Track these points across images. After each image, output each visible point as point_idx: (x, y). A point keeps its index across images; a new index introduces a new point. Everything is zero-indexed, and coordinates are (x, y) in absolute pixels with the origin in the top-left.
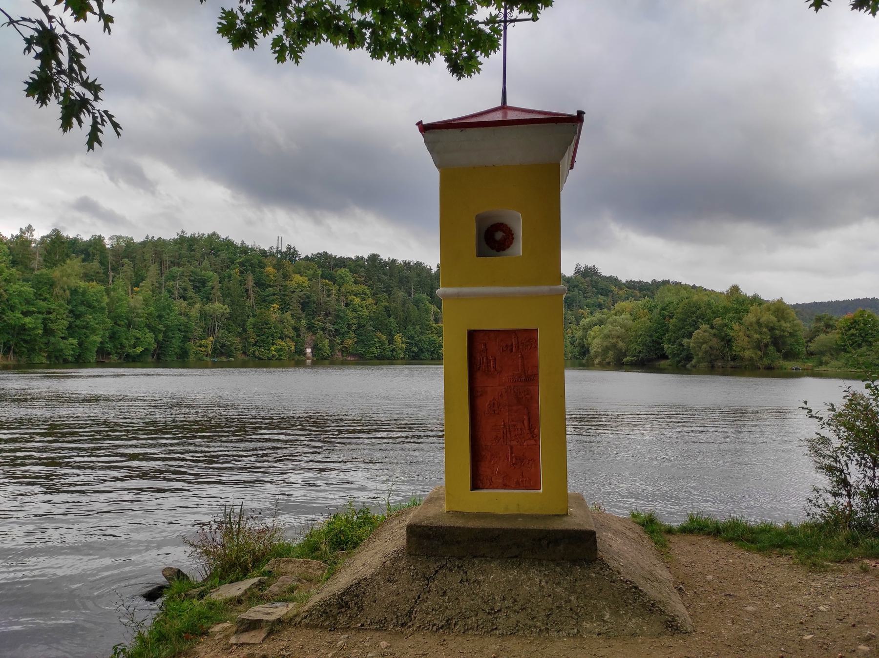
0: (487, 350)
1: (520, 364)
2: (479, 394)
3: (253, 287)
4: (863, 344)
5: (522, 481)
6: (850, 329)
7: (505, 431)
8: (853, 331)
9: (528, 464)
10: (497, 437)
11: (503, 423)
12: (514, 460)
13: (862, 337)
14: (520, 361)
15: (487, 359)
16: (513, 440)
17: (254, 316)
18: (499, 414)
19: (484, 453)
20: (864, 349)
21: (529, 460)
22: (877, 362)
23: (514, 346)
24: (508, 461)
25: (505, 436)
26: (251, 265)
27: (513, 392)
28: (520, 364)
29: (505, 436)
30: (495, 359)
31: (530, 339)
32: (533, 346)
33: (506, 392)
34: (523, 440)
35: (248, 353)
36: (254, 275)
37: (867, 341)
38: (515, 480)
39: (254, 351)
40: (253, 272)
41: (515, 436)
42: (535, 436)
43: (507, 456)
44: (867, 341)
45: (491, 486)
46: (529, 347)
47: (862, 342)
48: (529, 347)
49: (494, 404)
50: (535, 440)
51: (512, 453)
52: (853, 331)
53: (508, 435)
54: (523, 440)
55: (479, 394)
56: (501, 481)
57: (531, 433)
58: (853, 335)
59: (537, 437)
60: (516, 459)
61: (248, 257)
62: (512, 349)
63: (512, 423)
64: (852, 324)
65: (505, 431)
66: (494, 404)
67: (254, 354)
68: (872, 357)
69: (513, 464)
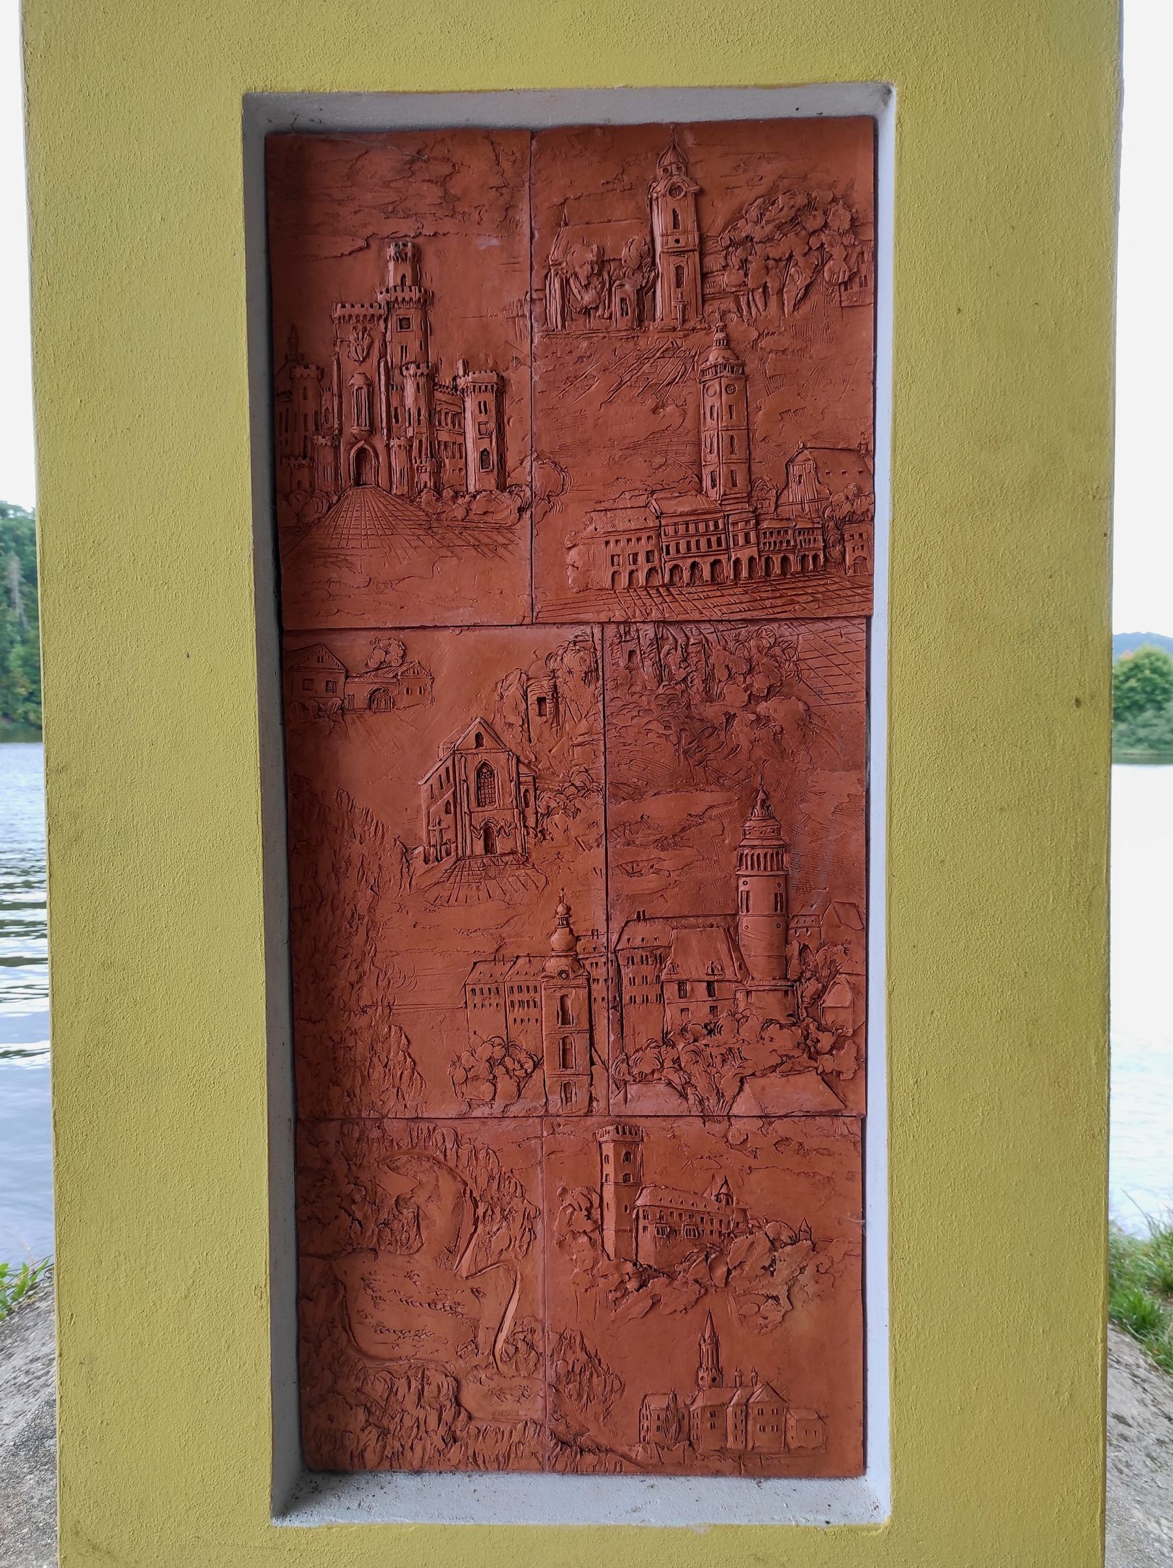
0: (426, 302)
1: (711, 428)
2: (359, 690)
3: (21, 584)
4: (1149, 706)
5: (715, 1412)
6: (1128, 679)
7: (575, 1000)
8: (1132, 683)
9: (769, 1270)
10: (509, 1046)
11: (557, 939)
12: (648, 1247)
13: (1146, 692)
14: (714, 400)
15: (431, 381)
16: (643, 1079)
17: (24, 642)
18: (524, 859)
19: (394, 1185)
20: (1149, 714)
21: (774, 1244)
22: (1168, 737)
23: (664, 266)
24: (597, 1244)
25: (579, 1044)
26: (16, 539)
27: (647, 671)
28: (711, 428)
29: (579, 1044)
30: (501, 389)
31: (810, 205)
32: (836, 268)
33: (591, 674)
34: (729, 1071)
35: (15, 716)
36: (22, 559)
37: (1154, 701)
38: (657, 1403)
39: (26, 713)
40: (20, 554)
41: (666, 1040)
42: (826, 1041)
43: (593, 1211)
44: (1154, 701)
45: (455, 1453)
46: (798, 279)
47: (1146, 702)
48: (798, 279)
49: (484, 771)
50: (830, 1079)
51: (630, 1183)
52: (1132, 683)
53: (605, 1037)
54: (729, 1071)
55: (359, 690)
56: (534, 1408)
57: (794, 1018)
58: (1132, 689)
59: (848, 1052)
60: (668, 1233)
61: (8, 523)
62: (645, 292)
63: (640, 933)
64: (1131, 670)
65: (575, 1000)
66: (484, 771)
67: (26, 718)
68: (1161, 730)
69: (644, 1276)
